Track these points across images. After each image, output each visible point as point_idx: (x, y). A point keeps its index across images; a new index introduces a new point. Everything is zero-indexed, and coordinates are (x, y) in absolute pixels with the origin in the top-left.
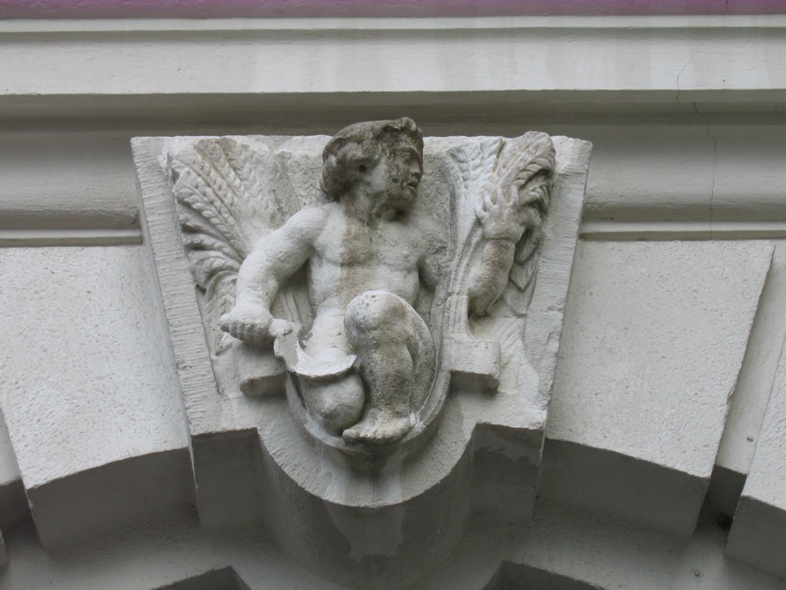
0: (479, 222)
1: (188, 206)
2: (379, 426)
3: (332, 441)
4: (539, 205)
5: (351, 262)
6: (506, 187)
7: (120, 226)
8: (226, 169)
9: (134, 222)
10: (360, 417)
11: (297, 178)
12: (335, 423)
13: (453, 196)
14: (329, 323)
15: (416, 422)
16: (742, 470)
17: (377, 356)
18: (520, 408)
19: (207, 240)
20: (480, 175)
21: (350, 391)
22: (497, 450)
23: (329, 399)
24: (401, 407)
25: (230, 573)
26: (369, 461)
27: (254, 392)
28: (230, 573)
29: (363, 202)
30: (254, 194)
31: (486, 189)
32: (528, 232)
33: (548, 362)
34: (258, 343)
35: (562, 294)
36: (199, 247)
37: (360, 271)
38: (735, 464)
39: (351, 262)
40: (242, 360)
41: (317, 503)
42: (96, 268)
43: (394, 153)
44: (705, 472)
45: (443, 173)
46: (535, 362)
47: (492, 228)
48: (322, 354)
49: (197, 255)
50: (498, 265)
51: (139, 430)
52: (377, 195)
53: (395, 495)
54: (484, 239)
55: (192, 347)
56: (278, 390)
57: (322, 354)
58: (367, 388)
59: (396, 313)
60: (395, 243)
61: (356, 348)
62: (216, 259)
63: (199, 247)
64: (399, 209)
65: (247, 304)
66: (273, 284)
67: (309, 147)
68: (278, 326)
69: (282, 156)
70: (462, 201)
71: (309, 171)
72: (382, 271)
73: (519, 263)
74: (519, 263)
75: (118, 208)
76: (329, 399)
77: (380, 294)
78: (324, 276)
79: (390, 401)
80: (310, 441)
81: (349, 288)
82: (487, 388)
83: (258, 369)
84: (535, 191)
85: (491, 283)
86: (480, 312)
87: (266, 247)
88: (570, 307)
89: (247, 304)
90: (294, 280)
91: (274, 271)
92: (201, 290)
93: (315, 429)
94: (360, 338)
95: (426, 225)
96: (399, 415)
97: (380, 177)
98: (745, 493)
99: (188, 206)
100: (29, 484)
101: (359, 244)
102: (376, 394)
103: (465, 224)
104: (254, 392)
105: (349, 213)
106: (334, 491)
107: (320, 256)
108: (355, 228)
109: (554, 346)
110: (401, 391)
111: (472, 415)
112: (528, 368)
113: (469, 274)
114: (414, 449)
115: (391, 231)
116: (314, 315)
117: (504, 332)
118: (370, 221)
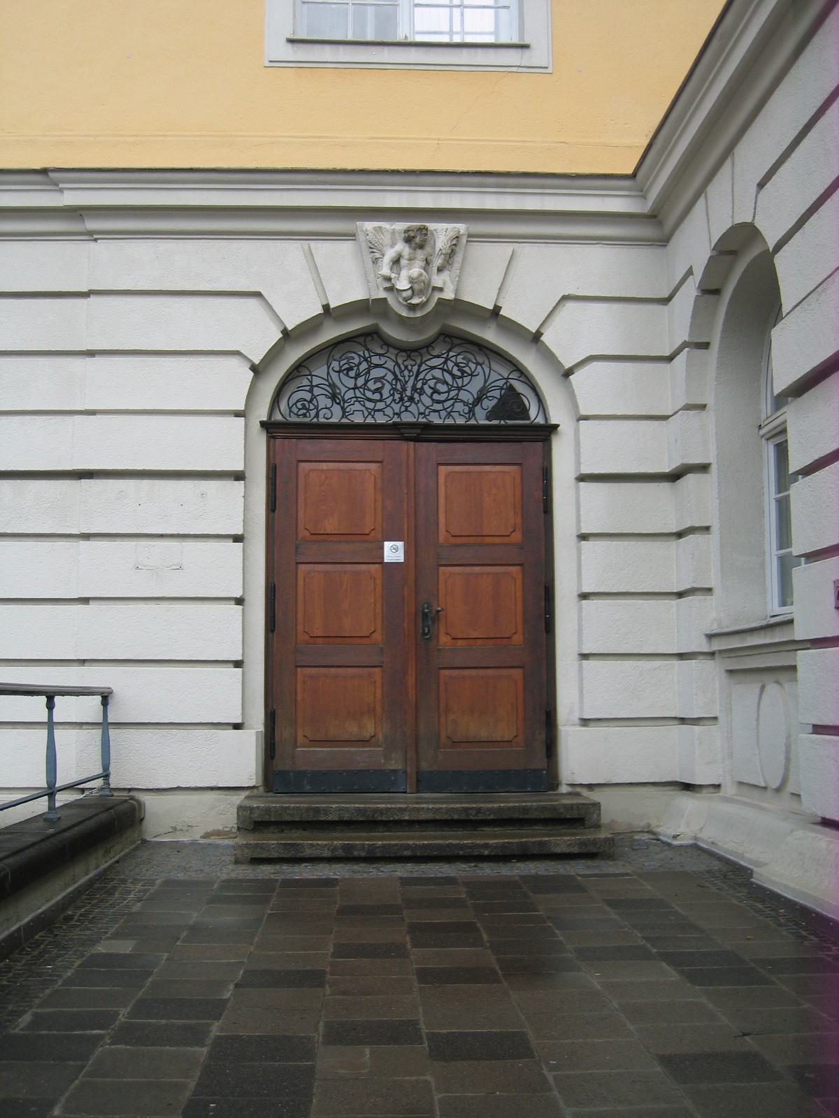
0: (441, 250)
1: (371, 243)
2: (415, 301)
3: (405, 303)
4: (455, 245)
5: (410, 260)
6: (448, 242)
7: (351, 236)
8: (380, 233)
9: (354, 235)
10: (411, 298)
11: (397, 235)
12: (406, 299)
13: (435, 241)
14: (404, 273)
15: (424, 299)
16: (529, 43)
17: (416, 285)
18: (449, 295)
19: (375, 251)
20: (442, 232)
21: (409, 292)
22: (441, 302)
23: (405, 294)
24: (421, 296)
25: (376, 325)
26: (413, 308)
27: (386, 289)
28: (376, 325)
29: (413, 245)
30: (386, 239)
31: (443, 241)
32: (452, 250)
33: (455, 283)
34: (388, 279)
35: (459, 266)
36: (373, 252)
37: (412, 262)
38: (499, 304)
39: (410, 260)
40: (384, 282)
41: (400, 315)
42: (346, 247)
43: (421, 234)
44: (491, 308)
45: (432, 234)
46: (452, 283)
47: (444, 252)
48: (403, 284)
49: (373, 254)
50: (445, 260)
51: (356, 293)
52: (416, 244)
53: (419, 314)
54: (442, 254)
55: (371, 277)
56: (391, 289)
57: (403, 284)
58: (413, 291)
59: (421, 275)
60: (420, 255)
61: (411, 282)
62: (377, 255)
63: (373, 252)
64: (421, 247)
65: (385, 270)
66: (391, 263)
67: (401, 226)
68: (393, 276)
69: (394, 229)
70: (437, 243)
71: (400, 233)
72: (417, 261)
73: (450, 258)
74: (450, 258)
75: (350, 232)
76: (405, 294)
77: (416, 271)
78: (403, 262)
79: (418, 295)
80: (400, 302)
81: (410, 267)
82: (441, 290)
83: (388, 285)
84: (454, 242)
85: (443, 264)
86: (440, 270)
87: (390, 254)
88: (462, 269)
89: (385, 270)
90: (396, 261)
91: (391, 261)
92: (373, 262)
93: (401, 300)
94: (412, 280)
95: (428, 249)
96: (421, 298)
97: (418, 240)
98: (501, 313)
99: (371, 243)
100: (332, 306)
101: (412, 256)
102: (415, 293)
103: (437, 250)
104: (386, 289)
105: (410, 247)
106: (404, 313)
107: (403, 257)
108: (411, 251)
109: (457, 279)
110: (421, 293)
111: (437, 296)
112: (450, 285)
113: (438, 262)
114: (422, 305)
115: (419, 252)
116: (401, 270)
117: (445, 276)
118: (415, 249)
